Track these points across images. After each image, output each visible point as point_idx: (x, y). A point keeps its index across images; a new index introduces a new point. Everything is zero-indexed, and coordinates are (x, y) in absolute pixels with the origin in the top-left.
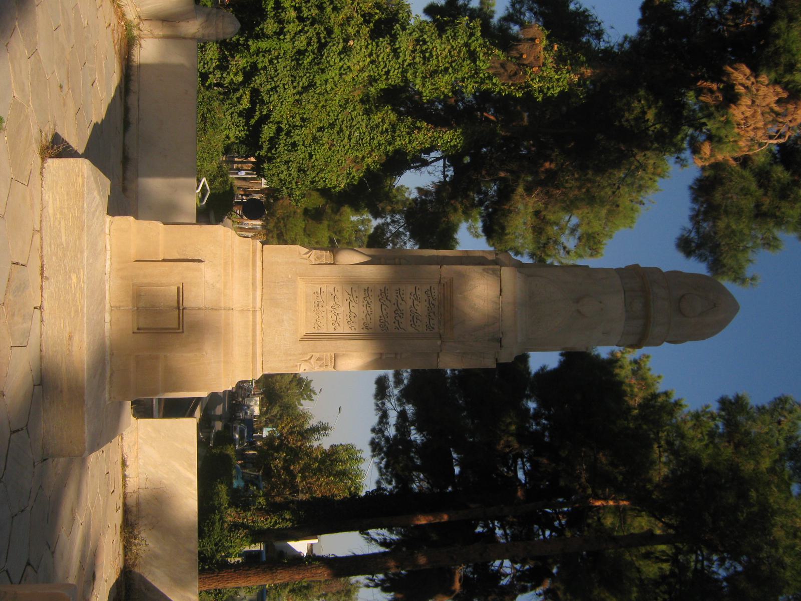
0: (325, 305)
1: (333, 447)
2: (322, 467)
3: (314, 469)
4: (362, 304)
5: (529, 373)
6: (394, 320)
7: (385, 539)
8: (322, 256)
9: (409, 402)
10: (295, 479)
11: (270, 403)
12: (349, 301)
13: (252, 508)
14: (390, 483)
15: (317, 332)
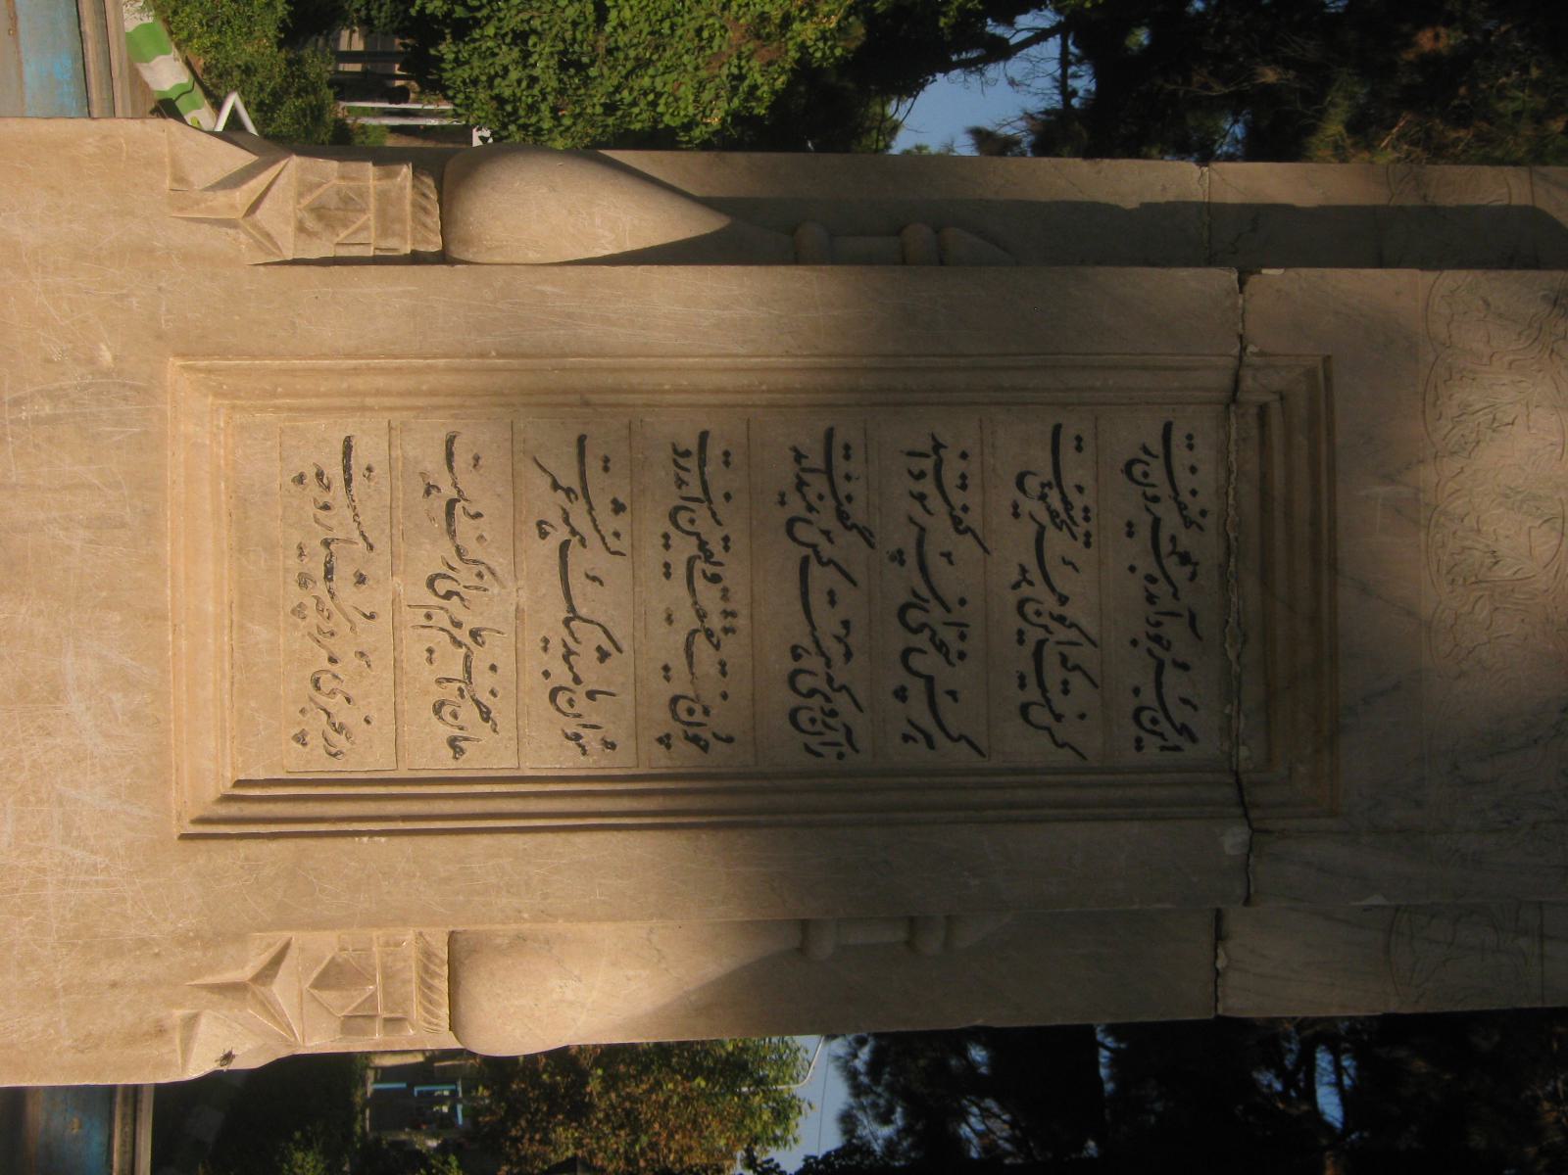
0: (377, 568)
4: (653, 554)
8: (350, 203)
10: (586, 1083)
12: (561, 534)
14: (885, 1119)
15: (313, 762)
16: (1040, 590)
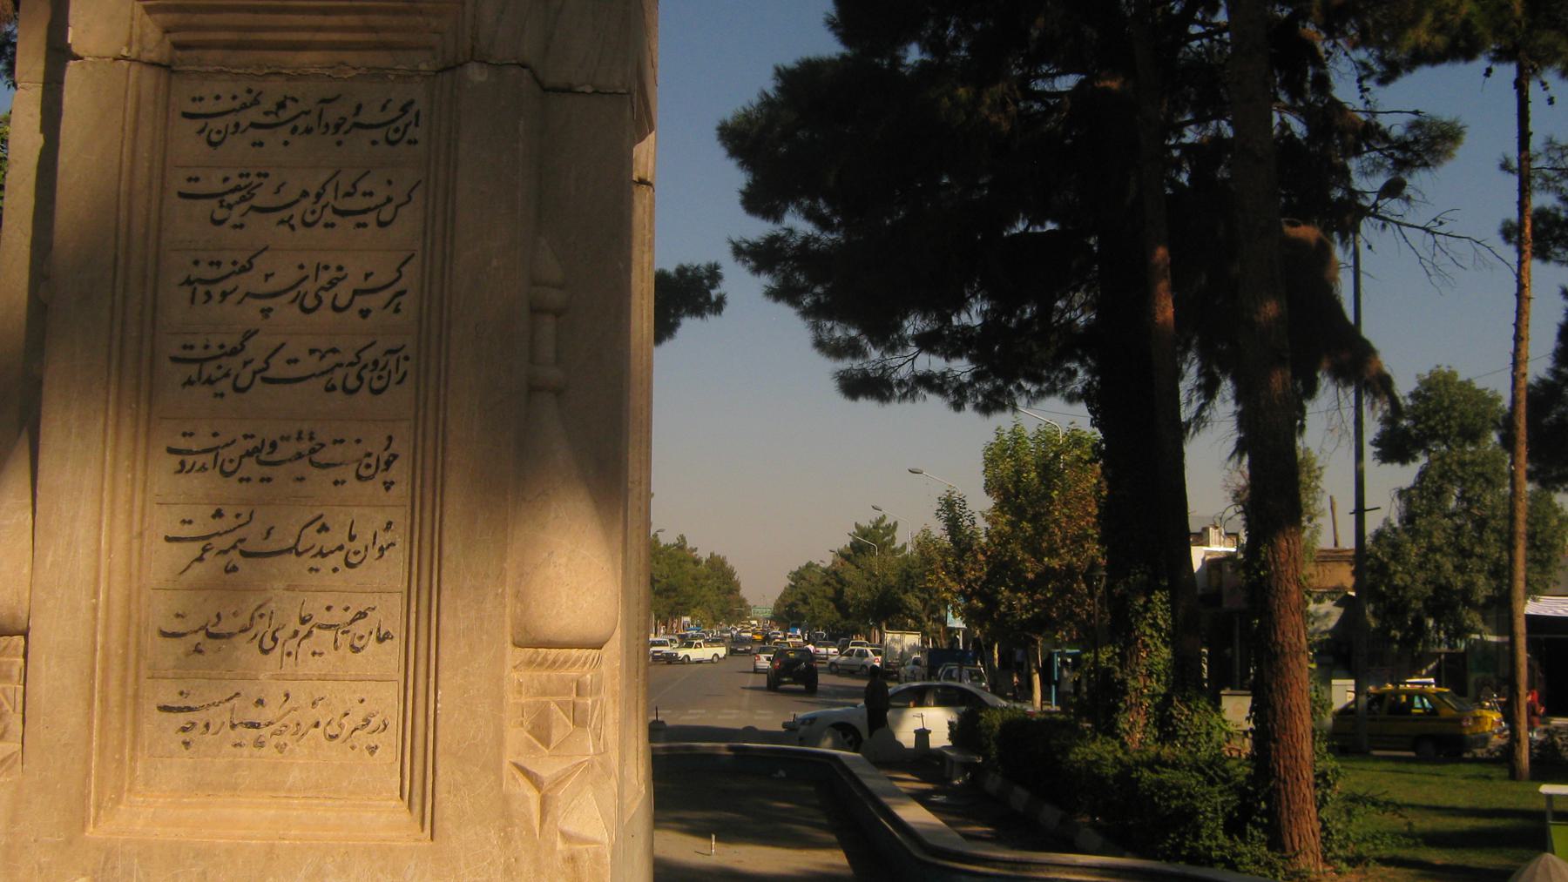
1: (988, 489)
2: (1030, 511)
3: (1035, 529)
5: (843, 57)
6: (352, 315)
7: (1199, 388)
9: (898, 327)
11: (899, 610)
13: (1119, 675)
14: (1074, 373)
15: (391, 738)
16: (297, 211)
